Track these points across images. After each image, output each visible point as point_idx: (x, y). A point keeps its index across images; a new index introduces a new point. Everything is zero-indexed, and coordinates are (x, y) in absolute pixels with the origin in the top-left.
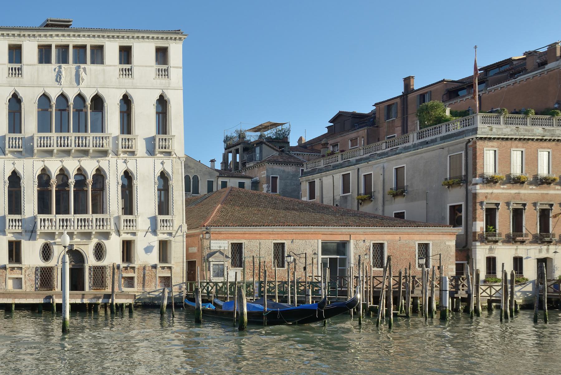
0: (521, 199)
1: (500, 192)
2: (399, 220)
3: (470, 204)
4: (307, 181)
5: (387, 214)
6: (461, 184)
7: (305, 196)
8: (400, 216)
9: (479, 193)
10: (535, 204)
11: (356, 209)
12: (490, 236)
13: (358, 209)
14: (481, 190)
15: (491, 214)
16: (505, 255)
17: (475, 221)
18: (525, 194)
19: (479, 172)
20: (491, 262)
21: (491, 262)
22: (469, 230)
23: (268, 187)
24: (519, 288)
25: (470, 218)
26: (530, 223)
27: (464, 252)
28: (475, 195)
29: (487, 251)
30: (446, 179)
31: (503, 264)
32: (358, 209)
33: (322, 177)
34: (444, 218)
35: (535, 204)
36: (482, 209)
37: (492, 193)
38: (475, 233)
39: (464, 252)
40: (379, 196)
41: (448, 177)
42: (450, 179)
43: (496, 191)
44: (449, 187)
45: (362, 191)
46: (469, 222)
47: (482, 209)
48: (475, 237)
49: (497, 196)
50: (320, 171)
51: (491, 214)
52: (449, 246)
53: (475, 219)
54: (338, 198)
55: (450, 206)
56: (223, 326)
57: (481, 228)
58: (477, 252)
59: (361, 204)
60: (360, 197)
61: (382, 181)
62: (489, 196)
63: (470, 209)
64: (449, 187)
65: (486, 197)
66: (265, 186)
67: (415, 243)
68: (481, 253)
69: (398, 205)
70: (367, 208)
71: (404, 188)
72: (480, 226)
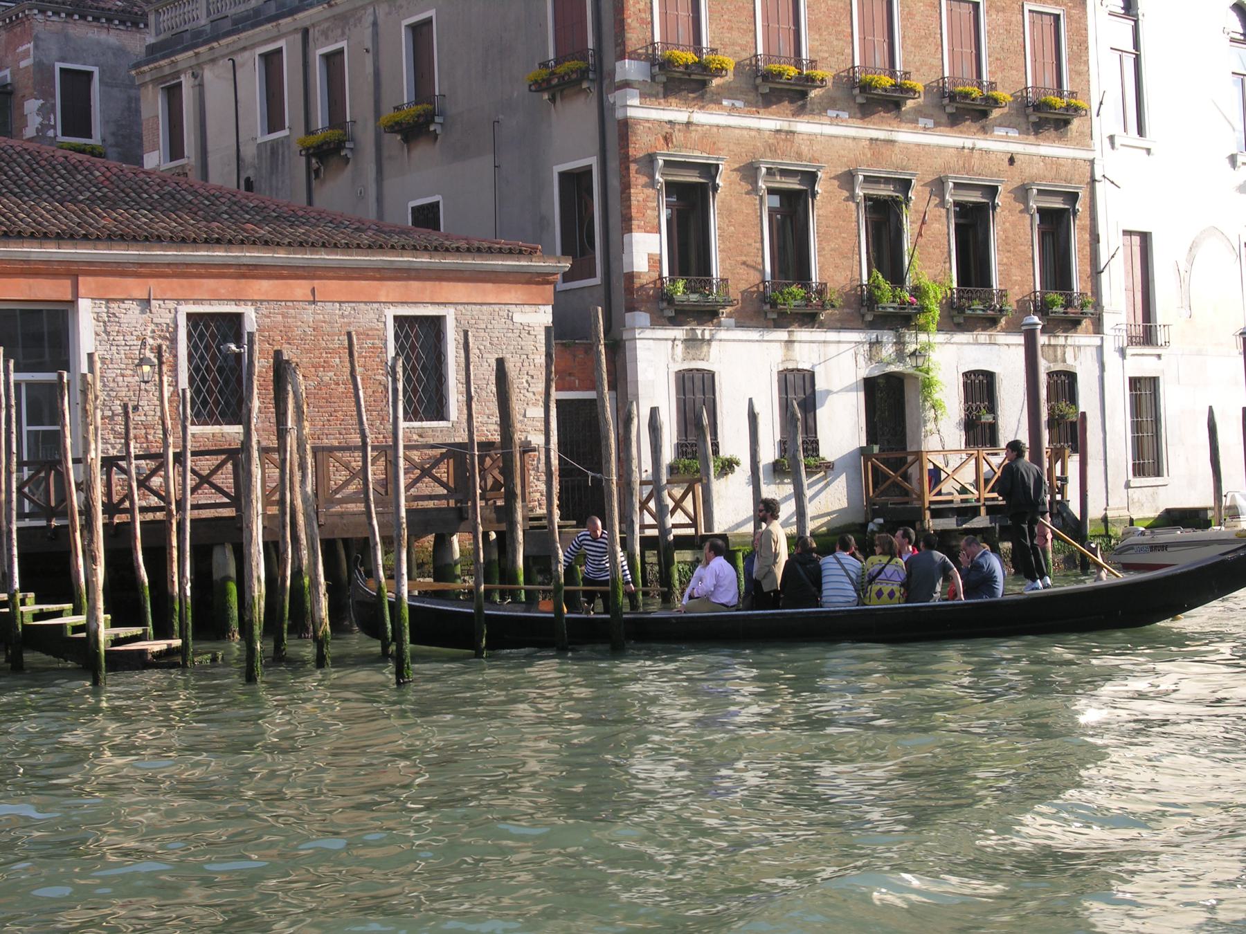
0: (799, 155)
1: (724, 127)
2: (423, 234)
3: (613, 164)
4: (156, 81)
5: (391, 219)
6: (585, 85)
7: (155, 147)
8: (427, 217)
9: (638, 121)
10: (847, 179)
11: (303, 201)
12: (690, 298)
13: (310, 202)
14: (643, 112)
15: (690, 205)
16: (746, 366)
17: (630, 231)
18: (812, 137)
19: (634, 38)
20: (696, 393)
21: (696, 393)
22: (614, 265)
23: (45, 111)
24: (353, 464)
25: (615, 220)
26: (837, 252)
27: (587, 347)
28: (625, 126)
29: (680, 347)
30: (544, 65)
31: (750, 400)
32: (310, 202)
33: (200, 65)
34: (543, 223)
35: (847, 179)
36: (652, 183)
37: (689, 124)
38: (631, 276)
39: (587, 347)
40: (366, 135)
41: (551, 56)
42: (558, 61)
43: (702, 117)
44: (553, 99)
45: (320, 119)
46: (614, 236)
47: (652, 183)
48: (623, 296)
49: (710, 136)
50: (197, 39)
51: (690, 205)
52: (527, 329)
53: (627, 225)
54: (249, 151)
55: (563, 175)
56: (578, 659)
57: (650, 257)
58: (641, 354)
59: (317, 172)
60: (314, 140)
61: (370, 79)
62: (678, 136)
63: (614, 182)
64: (553, 99)
65: (667, 139)
66: (32, 106)
67: (380, 318)
68: (656, 358)
69: (421, 179)
70: (335, 193)
71: (432, 103)
72: (647, 250)
